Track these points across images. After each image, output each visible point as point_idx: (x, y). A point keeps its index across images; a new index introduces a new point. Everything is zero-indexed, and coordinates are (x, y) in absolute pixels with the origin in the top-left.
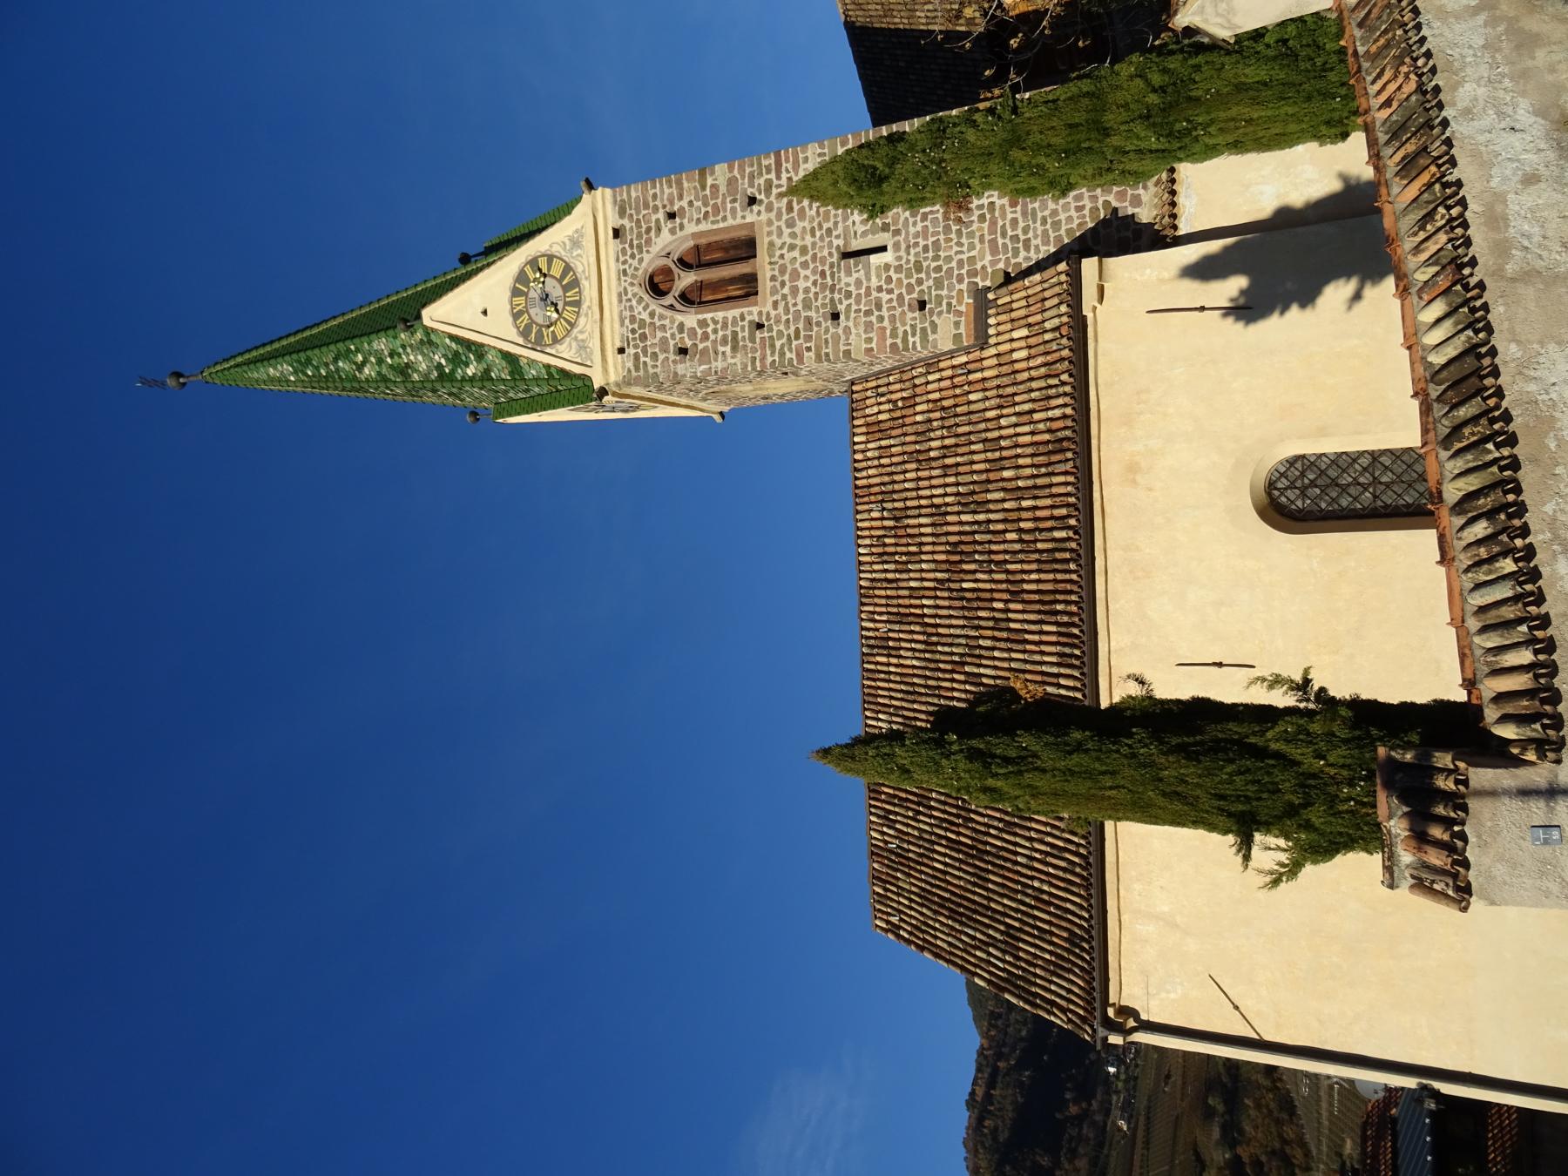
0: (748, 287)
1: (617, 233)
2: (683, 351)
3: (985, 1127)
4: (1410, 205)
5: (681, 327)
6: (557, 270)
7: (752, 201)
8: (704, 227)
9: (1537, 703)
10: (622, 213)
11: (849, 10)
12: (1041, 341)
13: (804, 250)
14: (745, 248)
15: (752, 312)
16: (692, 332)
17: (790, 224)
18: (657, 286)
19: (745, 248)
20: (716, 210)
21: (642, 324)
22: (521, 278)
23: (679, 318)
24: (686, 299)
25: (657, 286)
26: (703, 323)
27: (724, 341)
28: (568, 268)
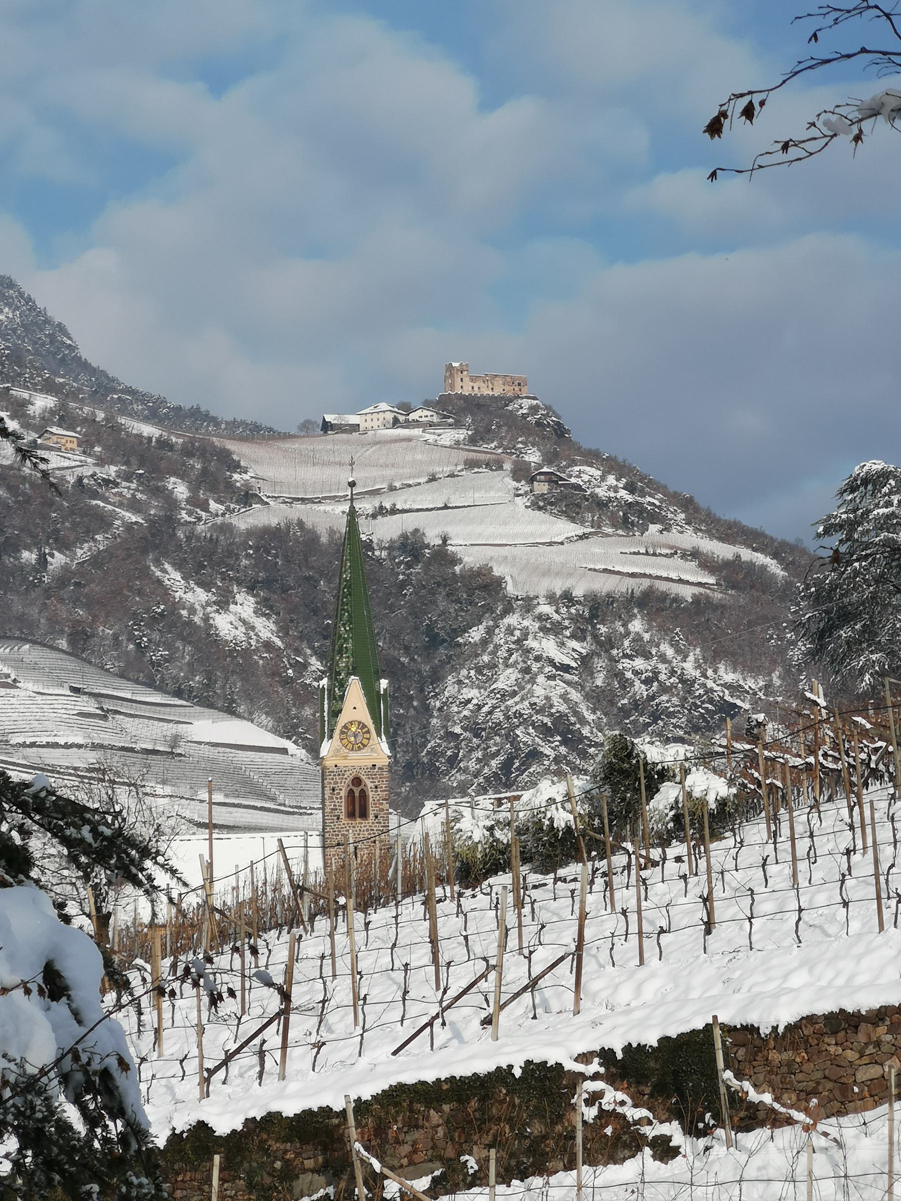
0: (351, 815)
1: (374, 766)
2: (333, 790)
3: (243, 1179)
4: (319, 1026)
5: (341, 790)
6: (365, 742)
7: (376, 817)
8: (371, 799)
9: (239, 1081)
10: (379, 768)
11: (226, 1190)
12: (278, 1055)
13: (359, 834)
14: (364, 815)
15: (342, 816)
16: (339, 794)
17: (367, 830)
18: (357, 781)
19: (364, 815)
20: (375, 804)
21: (344, 775)
22: (364, 726)
23: (344, 789)
24: (351, 792)
25: (357, 781)
26: (341, 798)
27: (335, 805)
28: (365, 746)
